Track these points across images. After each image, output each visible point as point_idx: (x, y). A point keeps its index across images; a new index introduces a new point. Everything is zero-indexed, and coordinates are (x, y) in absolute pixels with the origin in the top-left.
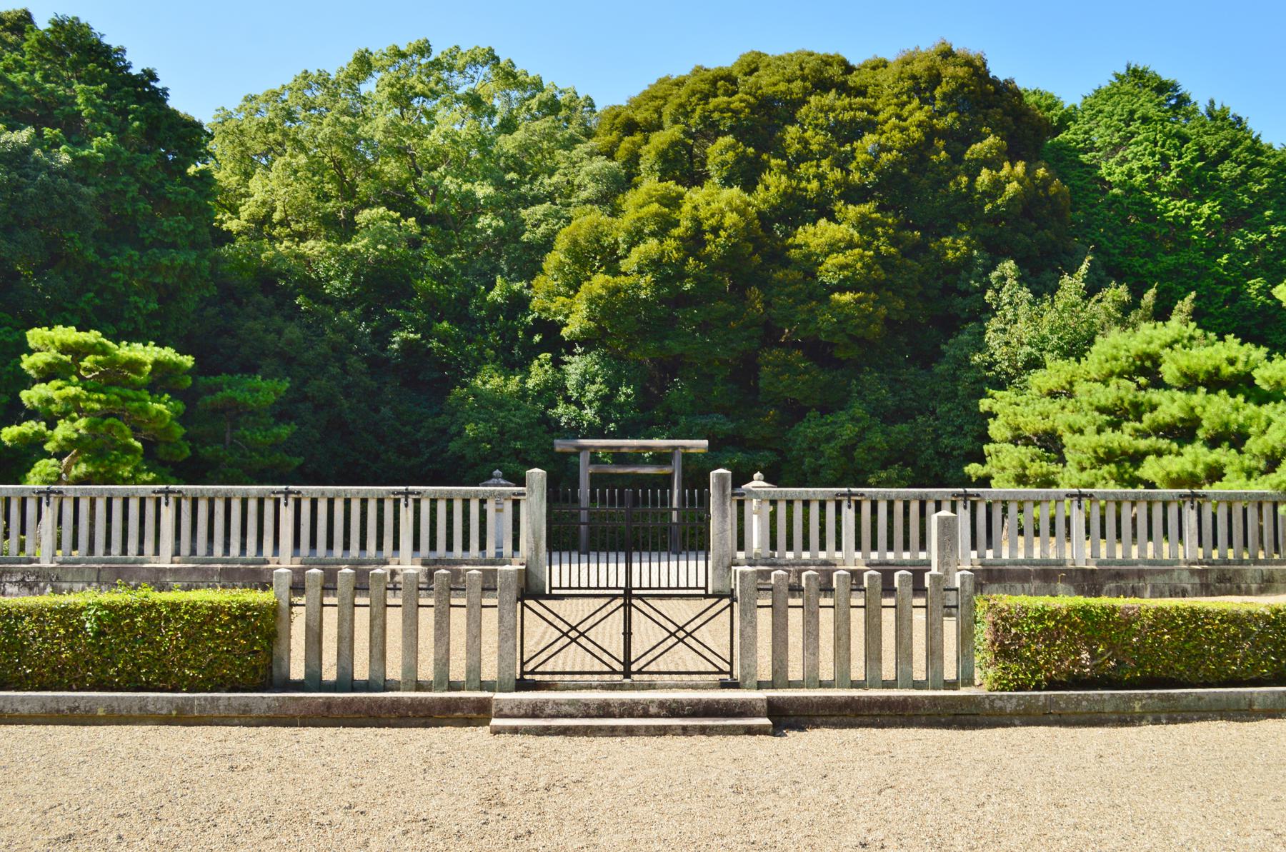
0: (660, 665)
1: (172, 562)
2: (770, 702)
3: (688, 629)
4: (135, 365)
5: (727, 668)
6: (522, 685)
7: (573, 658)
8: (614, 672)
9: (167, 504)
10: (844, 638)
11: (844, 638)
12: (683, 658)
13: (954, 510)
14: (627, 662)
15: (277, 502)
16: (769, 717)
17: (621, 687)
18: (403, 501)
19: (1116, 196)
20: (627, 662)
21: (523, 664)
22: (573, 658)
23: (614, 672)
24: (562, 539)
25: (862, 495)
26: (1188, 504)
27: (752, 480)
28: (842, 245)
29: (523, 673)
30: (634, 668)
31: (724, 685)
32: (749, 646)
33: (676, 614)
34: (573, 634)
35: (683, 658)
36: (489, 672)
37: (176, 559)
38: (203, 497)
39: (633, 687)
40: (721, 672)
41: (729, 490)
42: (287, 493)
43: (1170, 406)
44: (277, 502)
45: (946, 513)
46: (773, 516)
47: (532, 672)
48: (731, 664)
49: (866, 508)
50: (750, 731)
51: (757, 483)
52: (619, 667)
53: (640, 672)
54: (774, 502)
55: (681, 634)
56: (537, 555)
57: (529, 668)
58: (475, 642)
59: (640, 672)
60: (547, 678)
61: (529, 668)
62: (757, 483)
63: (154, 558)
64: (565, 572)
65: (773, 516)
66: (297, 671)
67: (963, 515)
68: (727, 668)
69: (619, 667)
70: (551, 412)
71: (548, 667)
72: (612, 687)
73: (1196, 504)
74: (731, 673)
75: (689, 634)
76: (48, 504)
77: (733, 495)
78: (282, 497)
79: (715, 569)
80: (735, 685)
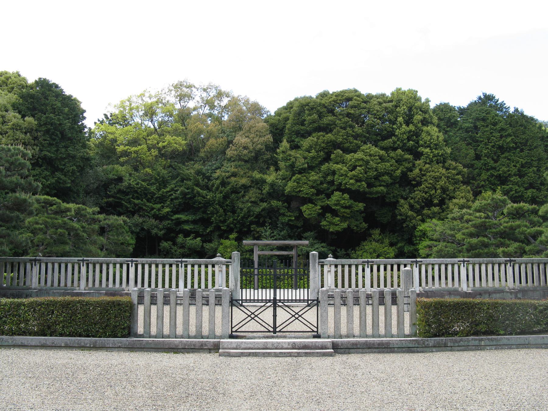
0: (289, 328)
1: (85, 290)
2: (333, 343)
3: (294, 318)
4: (69, 210)
5: (315, 330)
6: (231, 337)
7: (253, 326)
8: (269, 331)
9: (83, 266)
10: (363, 317)
11: (363, 317)
12: (297, 326)
13: (412, 268)
14: (275, 327)
15: (128, 265)
16: (333, 349)
17: (272, 337)
18: (180, 265)
19: (507, 324)
20: (275, 327)
21: (232, 328)
22: (253, 326)
23: (269, 331)
24: (247, 282)
25: (373, 262)
26: (509, 264)
27: (328, 257)
28: (91, 194)
29: (232, 332)
30: (278, 330)
31: (314, 337)
32: (325, 322)
33: (293, 310)
34: (253, 316)
35: (297, 326)
36: (218, 331)
37: (87, 288)
38: (98, 263)
39: (277, 337)
40: (313, 331)
41: (317, 261)
42: (132, 261)
43: (505, 223)
44: (128, 265)
45: (408, 268)
46: (336, 272)
47: (236, 331)
48: (317, 328)
49: (375, 268)
50: (324, 355)
51: (330, 259)
52: (272, 330)
53: (280, 331)
54: (336, 266)
55: (297, 316)
56: (236, 288)
57: (234, 330)
58: (211, 320)
59: (280, 331)
60: (242, 334)
61: (234, 330)
62: (330, 259)
63: (77, 288)
64: (248, 294)
65: (336, 272)
66: (140, 330)
67: (416, 271)
68: (315, 330)
69: (272, 330)
70: (409, 173)
71: (243, 329)
72: (268, 337)
73: (512, 264)
74: (317, 332)
75: (300, 316)
76: (35, 265)
77: (319, 262)
78: (130, 263)
79: (311, 294)
80: (318, 337)
